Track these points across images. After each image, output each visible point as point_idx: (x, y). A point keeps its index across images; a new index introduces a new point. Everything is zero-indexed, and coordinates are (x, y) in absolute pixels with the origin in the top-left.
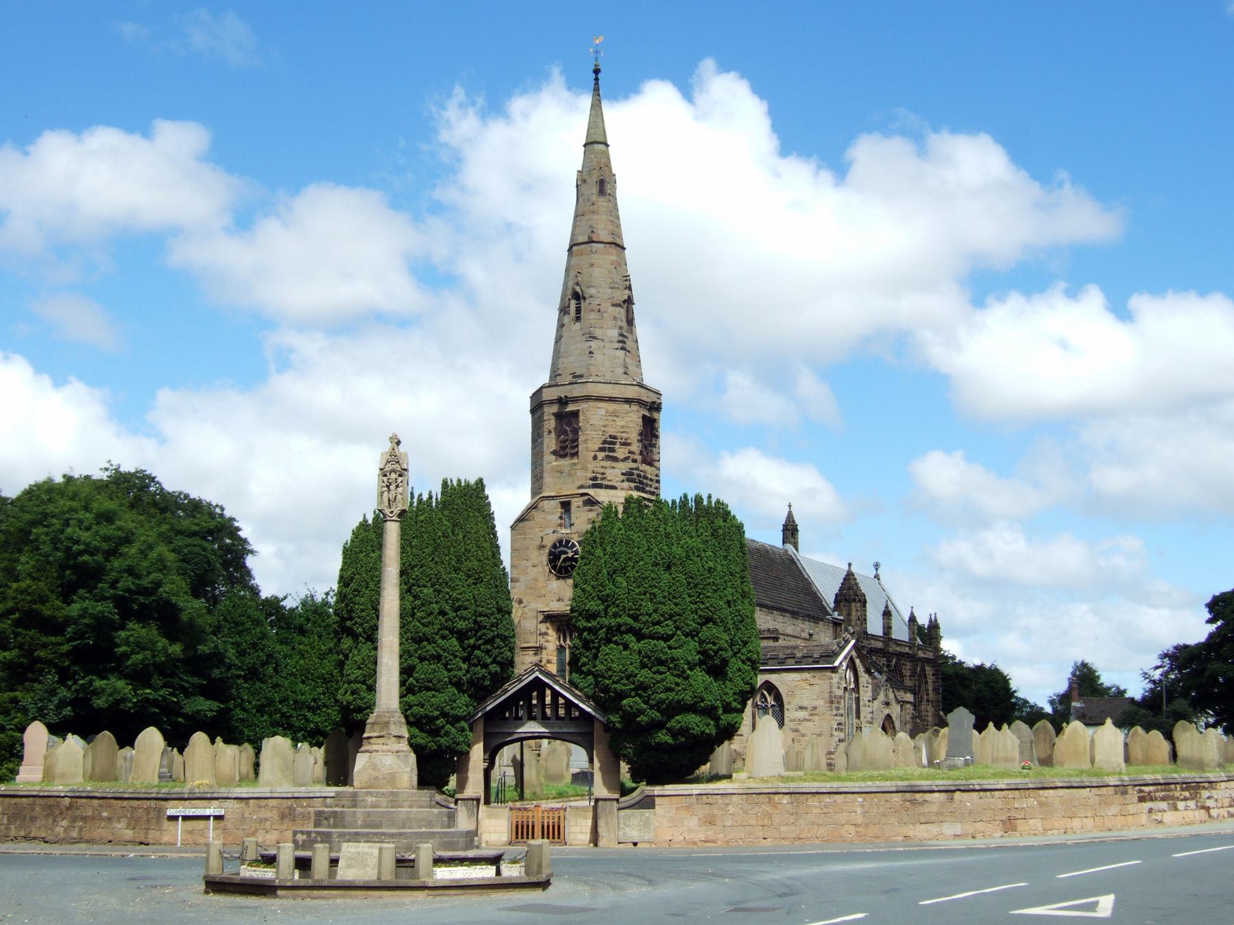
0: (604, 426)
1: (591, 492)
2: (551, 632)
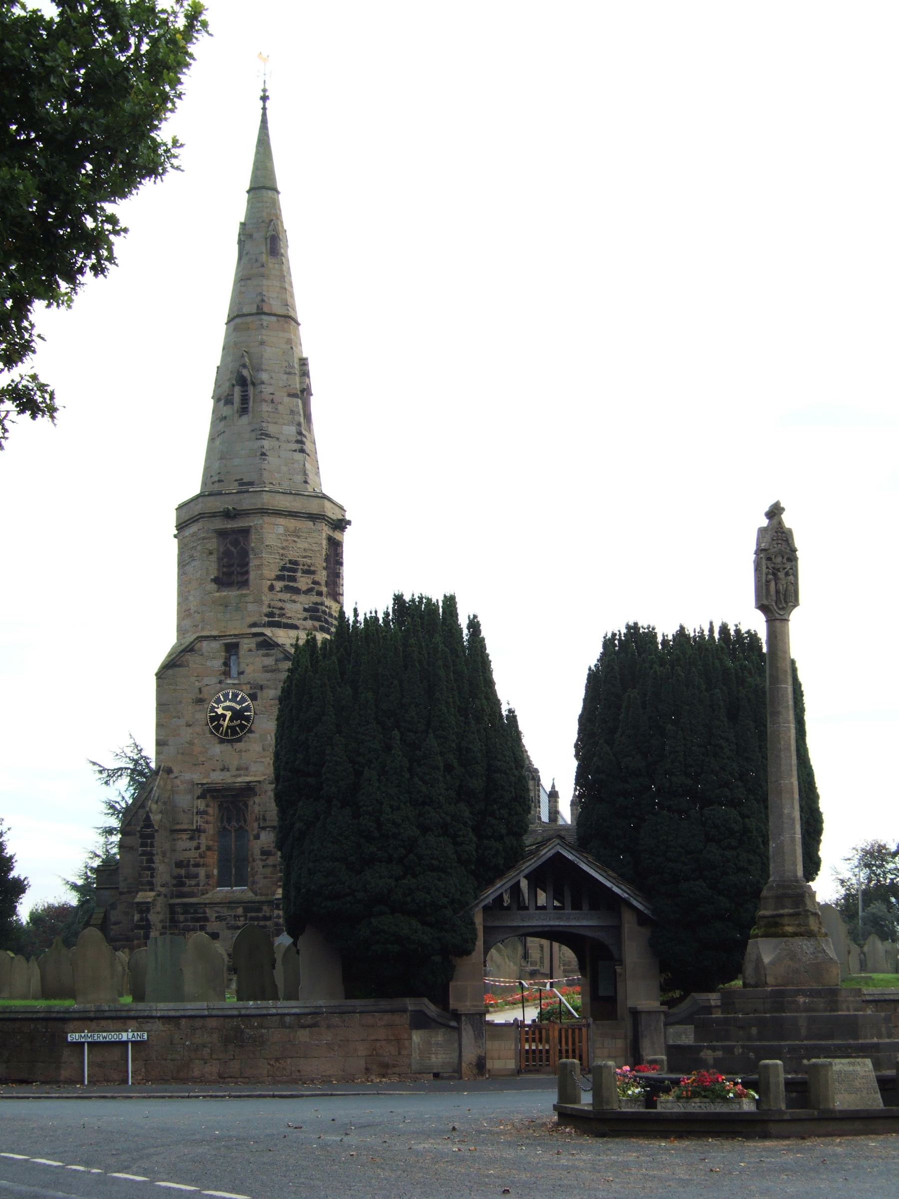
0: (283, 548)
1: (268, 631)
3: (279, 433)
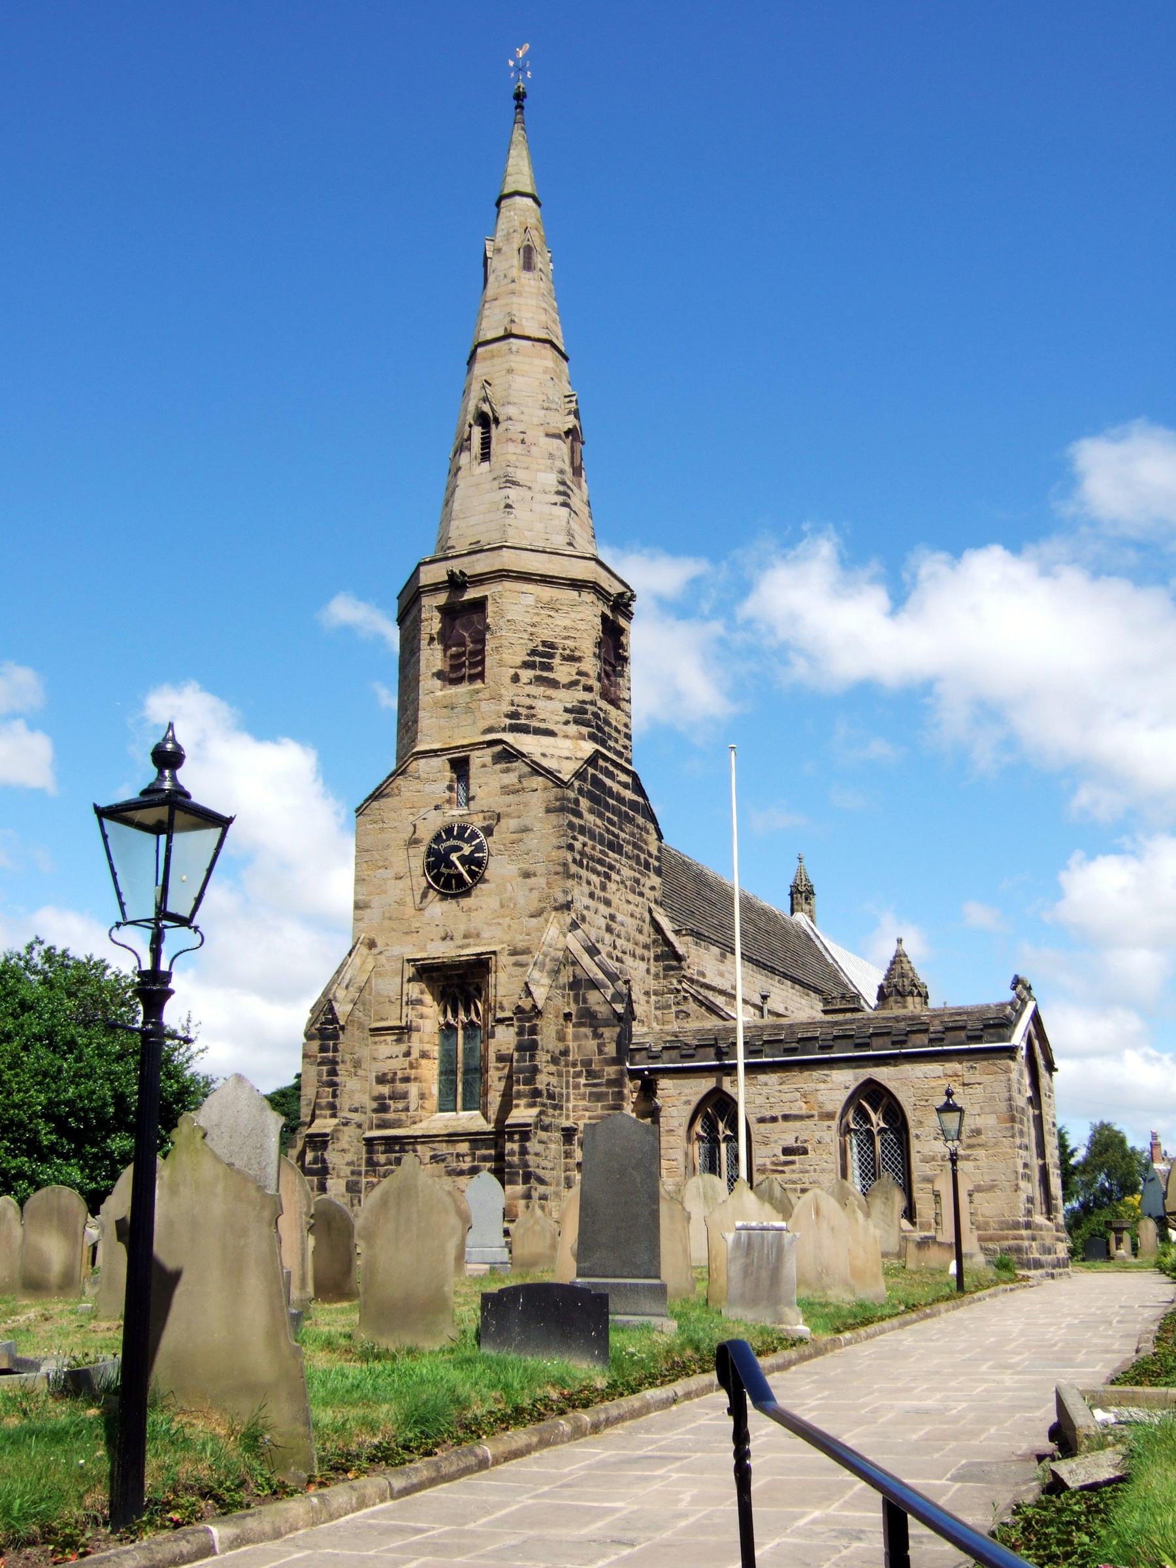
0: (533, 625)
1: (509, 737)
2: (428, 998)
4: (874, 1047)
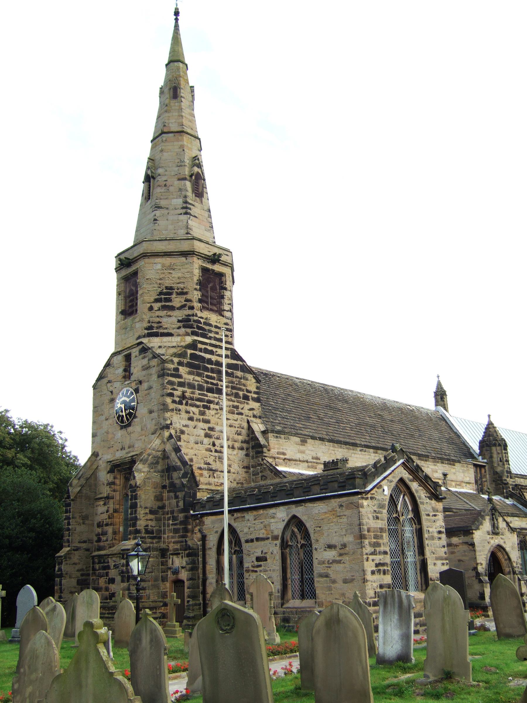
0: (160, 279)
1: (145, 340)
3: (168, 205)
4: (295, 496)
